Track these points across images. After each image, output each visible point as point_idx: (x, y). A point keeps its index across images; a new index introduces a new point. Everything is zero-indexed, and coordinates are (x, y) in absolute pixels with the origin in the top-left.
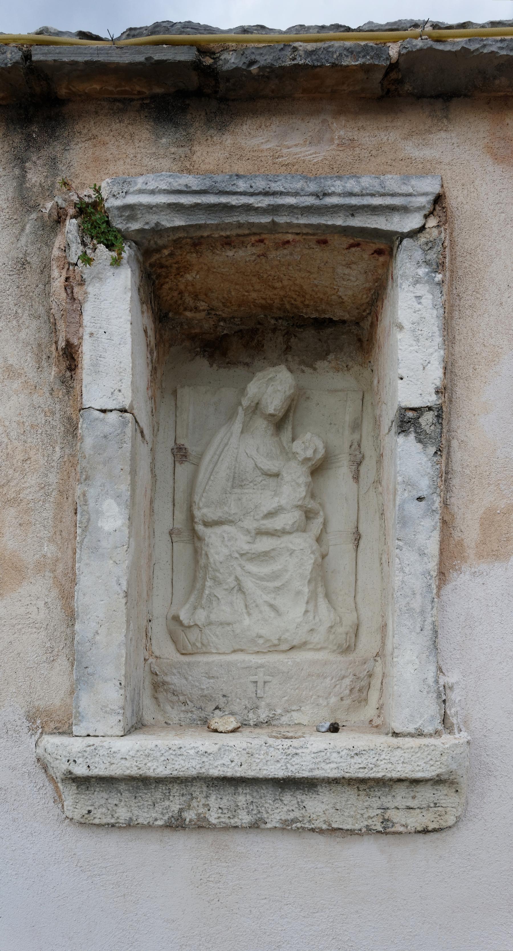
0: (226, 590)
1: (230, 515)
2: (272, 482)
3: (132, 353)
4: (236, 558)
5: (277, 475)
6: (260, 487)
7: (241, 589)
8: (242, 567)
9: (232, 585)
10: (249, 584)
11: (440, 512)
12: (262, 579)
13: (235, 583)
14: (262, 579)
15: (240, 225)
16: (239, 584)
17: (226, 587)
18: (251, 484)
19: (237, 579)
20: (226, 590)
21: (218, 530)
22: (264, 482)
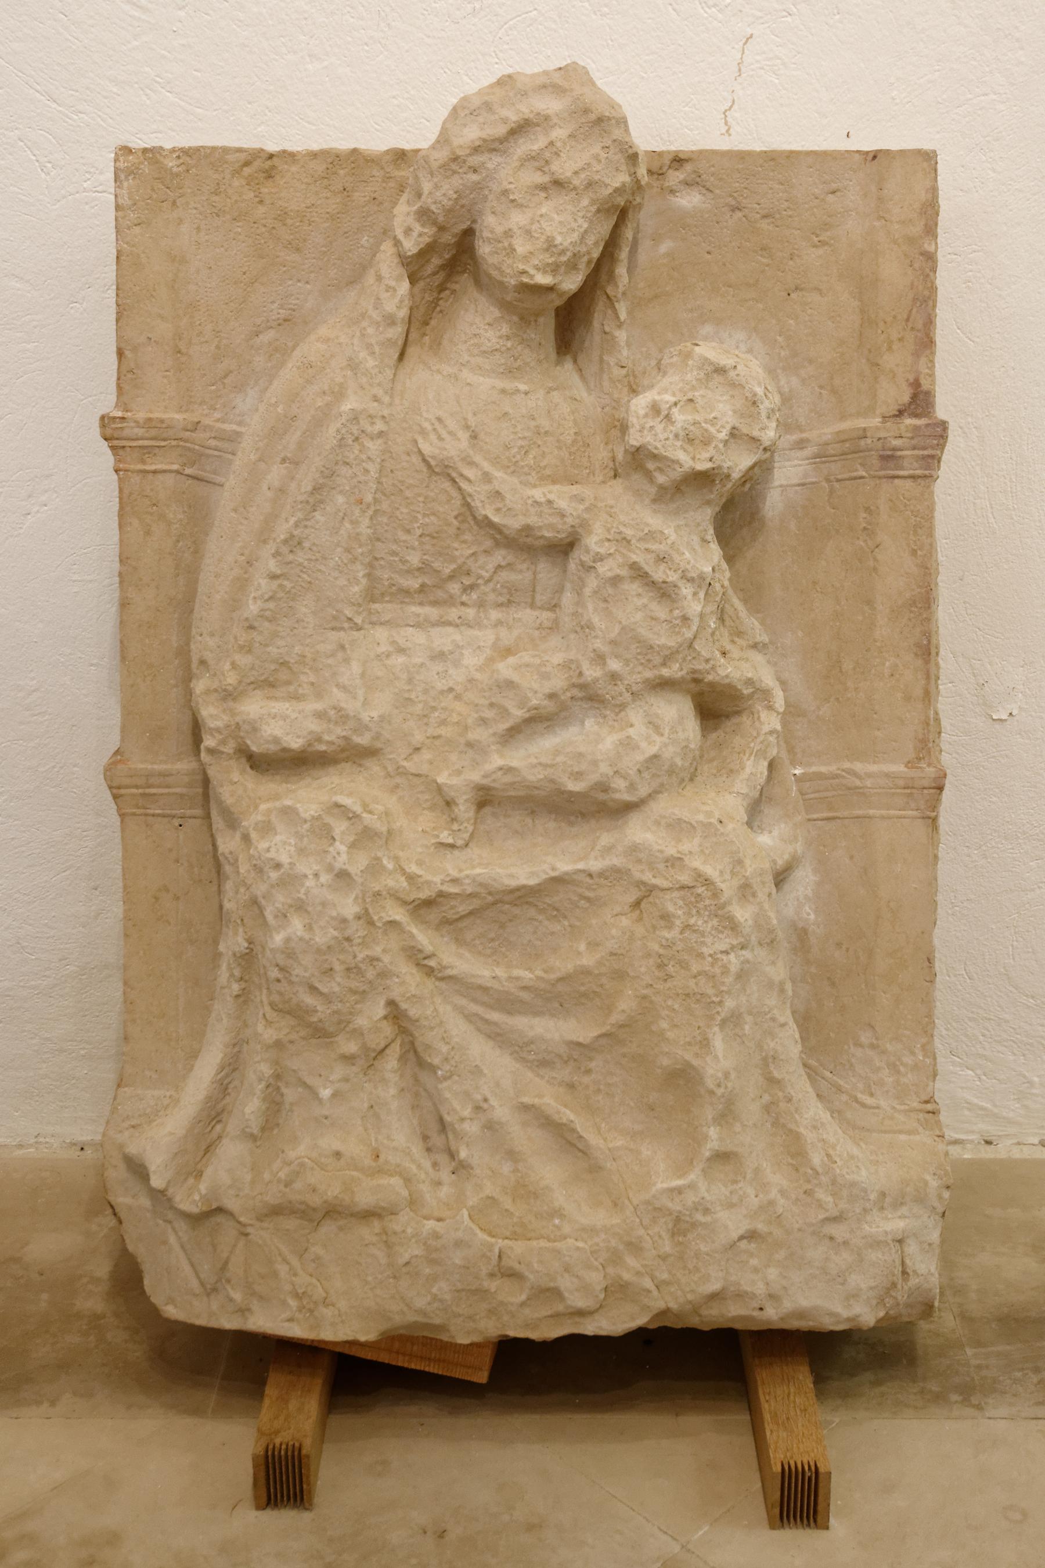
0: (349, 1059)
1: (361, 727)
2: (545, 571)
3: (121, 622)
4: (393, 924)
5: (563, 548)
6: (492, 597)
7: (415, 1056)
8: (418, 958)
9: (376, 1041)
10: (449, 1027)
11: (921, 1384)
12: (507, 1003)
13: (388, 1030)
14: (507, 1003)
15: (474, 1000)
16: (403, 1031)
17: (351, 1047)
18: (454, 588)
19: (395, 1014)
20: (349, 1059)
21: (308, 796)
22: (504, 575)
